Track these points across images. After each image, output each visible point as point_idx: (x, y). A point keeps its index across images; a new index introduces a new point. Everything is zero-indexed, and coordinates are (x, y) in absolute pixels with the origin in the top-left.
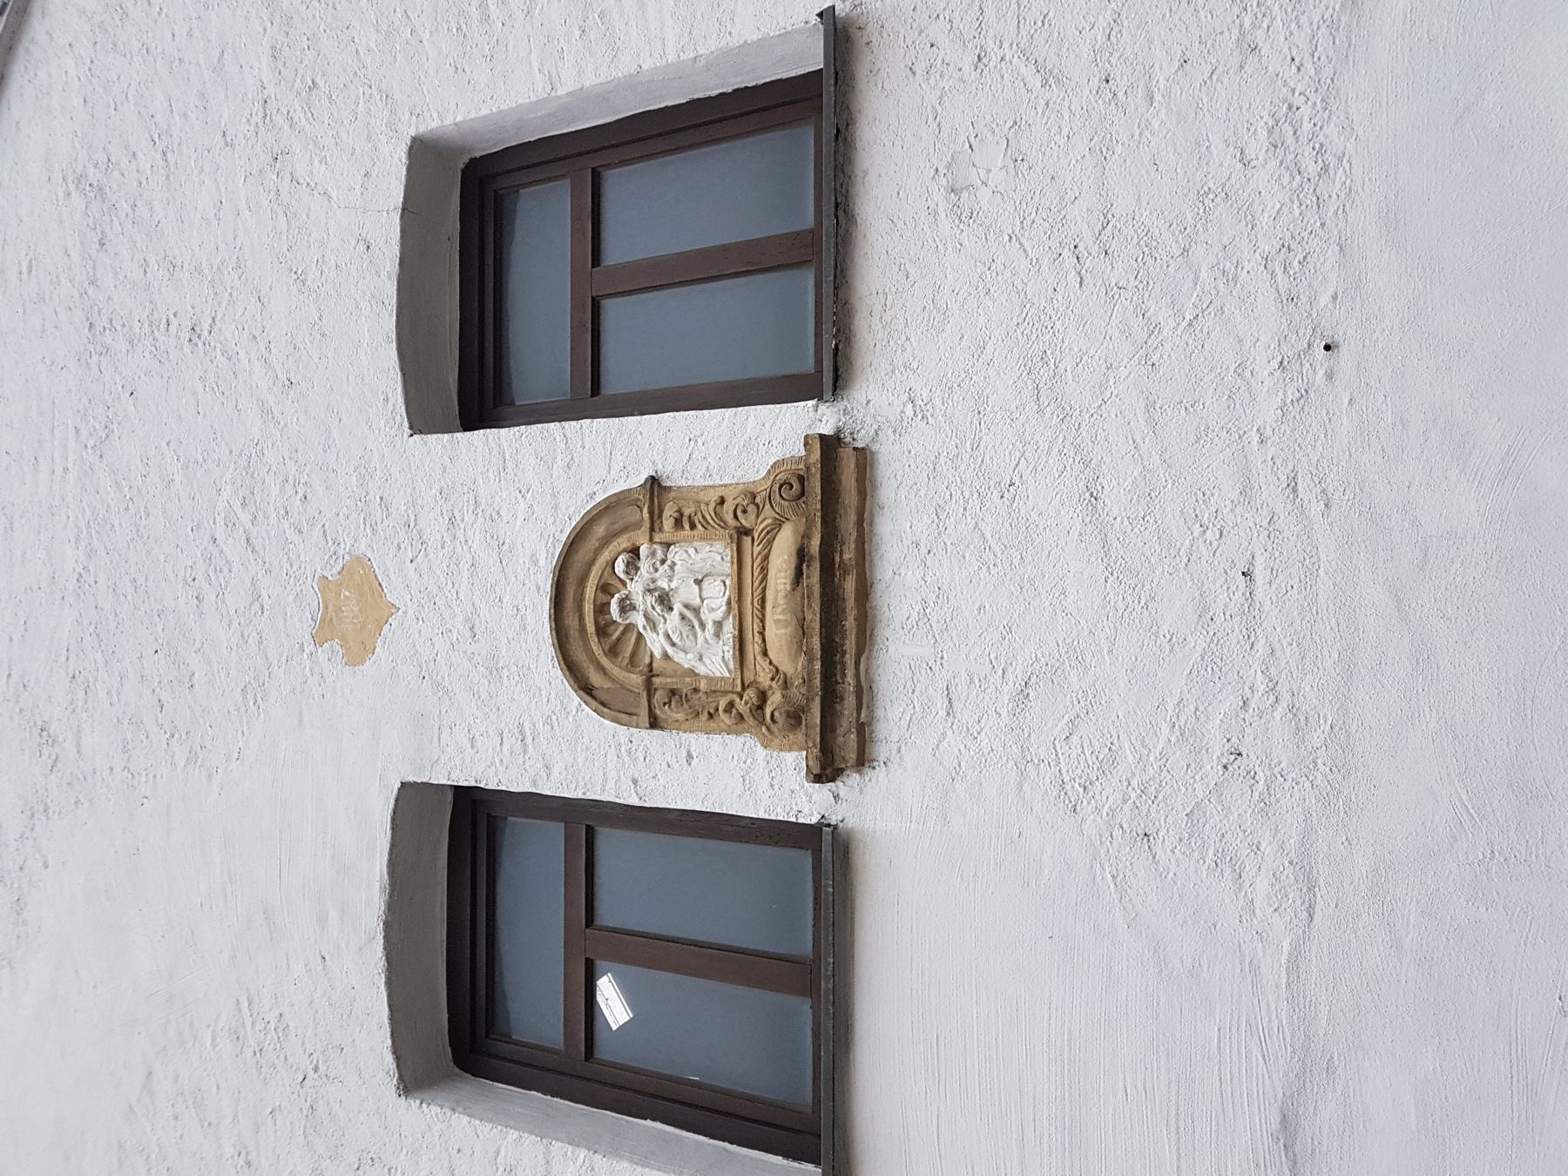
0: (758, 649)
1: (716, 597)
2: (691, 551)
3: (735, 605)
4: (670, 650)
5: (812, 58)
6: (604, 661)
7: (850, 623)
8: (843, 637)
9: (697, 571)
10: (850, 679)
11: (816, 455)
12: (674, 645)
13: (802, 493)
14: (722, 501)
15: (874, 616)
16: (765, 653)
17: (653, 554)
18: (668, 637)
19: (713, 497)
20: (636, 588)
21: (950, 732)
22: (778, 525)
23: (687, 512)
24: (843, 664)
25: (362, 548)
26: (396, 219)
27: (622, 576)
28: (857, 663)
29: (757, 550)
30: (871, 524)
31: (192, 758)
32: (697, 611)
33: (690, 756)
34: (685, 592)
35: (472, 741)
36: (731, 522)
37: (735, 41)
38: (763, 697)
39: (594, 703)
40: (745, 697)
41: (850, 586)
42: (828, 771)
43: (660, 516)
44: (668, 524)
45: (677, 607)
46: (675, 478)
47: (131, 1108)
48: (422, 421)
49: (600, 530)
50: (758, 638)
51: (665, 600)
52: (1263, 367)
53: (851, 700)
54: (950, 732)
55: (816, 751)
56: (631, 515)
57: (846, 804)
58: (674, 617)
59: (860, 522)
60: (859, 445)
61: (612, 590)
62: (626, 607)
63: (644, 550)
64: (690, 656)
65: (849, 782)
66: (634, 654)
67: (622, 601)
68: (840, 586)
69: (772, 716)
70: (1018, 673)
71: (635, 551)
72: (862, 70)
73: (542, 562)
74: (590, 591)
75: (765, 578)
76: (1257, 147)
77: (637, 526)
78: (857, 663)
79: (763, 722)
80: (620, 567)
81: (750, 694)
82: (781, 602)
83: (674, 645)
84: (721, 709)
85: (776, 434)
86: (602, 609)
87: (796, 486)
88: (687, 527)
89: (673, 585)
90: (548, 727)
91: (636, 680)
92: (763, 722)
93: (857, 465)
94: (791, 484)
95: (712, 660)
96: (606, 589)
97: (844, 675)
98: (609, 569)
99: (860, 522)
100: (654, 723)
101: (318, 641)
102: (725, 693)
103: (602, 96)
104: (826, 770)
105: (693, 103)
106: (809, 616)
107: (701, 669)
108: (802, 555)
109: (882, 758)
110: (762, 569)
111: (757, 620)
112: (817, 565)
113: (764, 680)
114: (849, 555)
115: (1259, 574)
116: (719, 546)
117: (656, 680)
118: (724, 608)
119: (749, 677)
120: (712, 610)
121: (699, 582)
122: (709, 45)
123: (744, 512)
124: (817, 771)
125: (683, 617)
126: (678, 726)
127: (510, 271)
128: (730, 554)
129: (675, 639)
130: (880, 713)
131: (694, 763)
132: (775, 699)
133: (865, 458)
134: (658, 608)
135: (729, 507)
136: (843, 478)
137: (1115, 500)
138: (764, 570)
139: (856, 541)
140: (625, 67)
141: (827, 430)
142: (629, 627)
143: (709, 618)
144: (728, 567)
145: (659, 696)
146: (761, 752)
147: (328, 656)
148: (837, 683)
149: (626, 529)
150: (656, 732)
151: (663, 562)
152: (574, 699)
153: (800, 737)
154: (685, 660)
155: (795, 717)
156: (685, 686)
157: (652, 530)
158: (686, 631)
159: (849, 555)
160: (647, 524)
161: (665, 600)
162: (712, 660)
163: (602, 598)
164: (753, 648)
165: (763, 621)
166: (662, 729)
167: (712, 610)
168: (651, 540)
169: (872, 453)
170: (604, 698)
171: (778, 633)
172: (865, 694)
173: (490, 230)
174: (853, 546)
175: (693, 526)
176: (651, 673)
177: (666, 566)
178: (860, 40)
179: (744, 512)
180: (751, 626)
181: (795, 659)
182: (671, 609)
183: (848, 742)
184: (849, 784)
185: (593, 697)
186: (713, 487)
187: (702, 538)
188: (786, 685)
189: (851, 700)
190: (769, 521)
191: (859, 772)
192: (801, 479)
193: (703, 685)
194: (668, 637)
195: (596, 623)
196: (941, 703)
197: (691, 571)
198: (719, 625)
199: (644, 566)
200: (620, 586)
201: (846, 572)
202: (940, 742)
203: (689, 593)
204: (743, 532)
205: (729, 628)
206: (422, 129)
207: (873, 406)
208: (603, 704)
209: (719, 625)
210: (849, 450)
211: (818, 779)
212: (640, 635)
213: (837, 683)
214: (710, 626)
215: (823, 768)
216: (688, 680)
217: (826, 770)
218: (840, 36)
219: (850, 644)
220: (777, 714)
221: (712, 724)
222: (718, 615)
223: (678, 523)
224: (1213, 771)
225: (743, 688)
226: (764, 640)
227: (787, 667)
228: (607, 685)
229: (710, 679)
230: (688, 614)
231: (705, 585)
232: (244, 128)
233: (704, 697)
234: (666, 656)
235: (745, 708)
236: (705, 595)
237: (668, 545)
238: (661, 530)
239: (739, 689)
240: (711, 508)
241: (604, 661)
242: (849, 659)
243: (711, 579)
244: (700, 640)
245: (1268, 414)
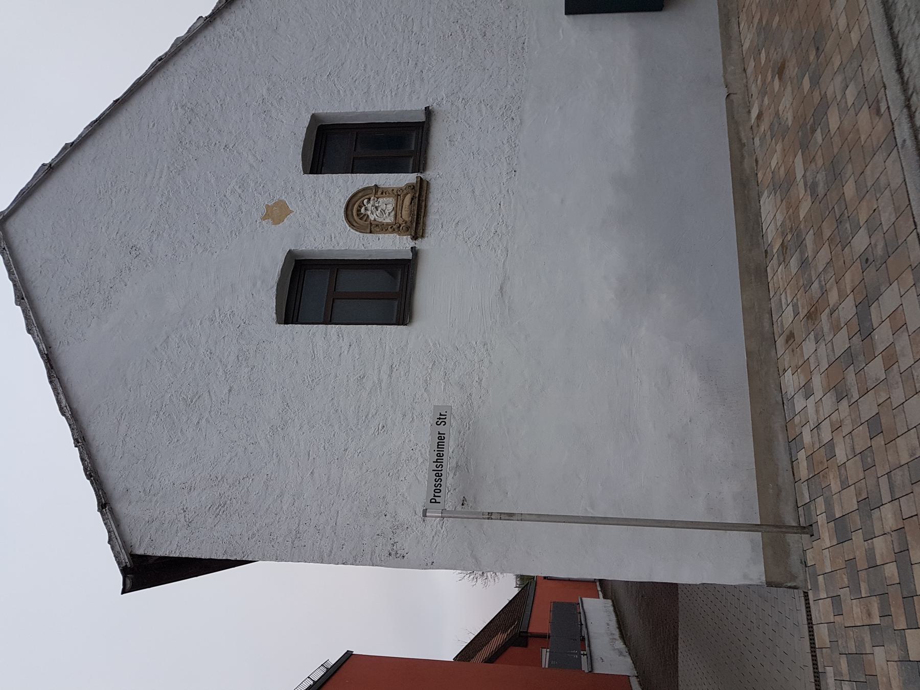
13: (521, 124)
31: (205, 250)
48: (305, 173)
52: (504, 173)
56: (369, 192)
57: (420, 244)
62: (366, 209)
70: (456, 221)
71: (369, 199)
72: (433, 119)
74: (356, 206)
85: (410, 178)
94: (411, 187)
100: (371, 232)
101: (264, 218)
103: (364, 114)
113: (401, 222)
126: (377, 232)
127: (332, 145)
137: (477, 193)
143: (387, 212)
155: (408, 229)
171: (405, 214)
180: (399, 212)
218: (428, 112)
224: (492, 235)
232: (254, 103)
235: (395, 228)
245: (505, 180)
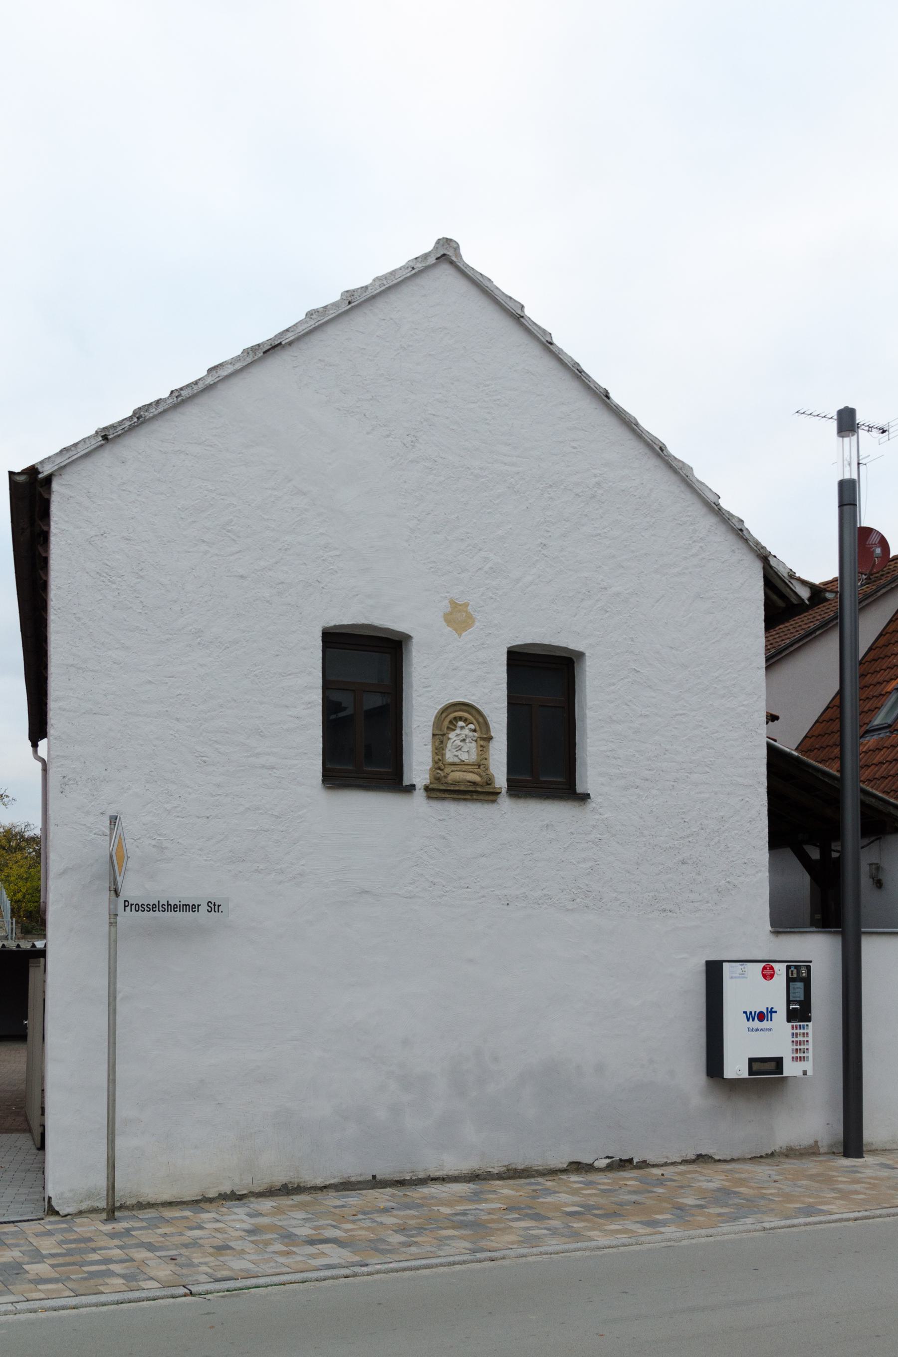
1: (464, 757)
5: (579, 789)
20: (466, 731)
22: (481, 776)
25: (477, 624)
26: (564, 645)
37: (589, 768)
38: (442, 770)
41: (468, 797)
44: (482, 743)
47: (290, 480)
49: (481, 720)
58: (458, 743)
62: (462, 728)
63: (476, 734)
71: (475, 731)
76: (545, 892)
86: (461, 719)
94: (489, 782)
96: (465, 720)
100: (434, 735)
104: (427, 789)
105: (575, 759)
115: (469, 890)
122: (589, 761)
126: (434, 742)
133: (494, 801)
140: (589, 733)
146: (429, 767)
147: (445, 606)
154: (449, 745)
155: (438, 779)
161: (464, 740)
164: (453, 768)
172: (444, 799)
173: (801, 643)
178: (582, 803)
180: (458, 768)
183: (434, 795)
184: (424, 794)
188: (445, 777)
189: (444, 796)
196: (441, 818)
199: (471, 734)
203: (465, 749)
204: (479, 766)
206: (587, 658)
207: (505, 803)
214: (456, 753)
217: (427, 789)
223: (482, 746)
234: (449, 739)
235: (439, 764)
245: (497, 892)
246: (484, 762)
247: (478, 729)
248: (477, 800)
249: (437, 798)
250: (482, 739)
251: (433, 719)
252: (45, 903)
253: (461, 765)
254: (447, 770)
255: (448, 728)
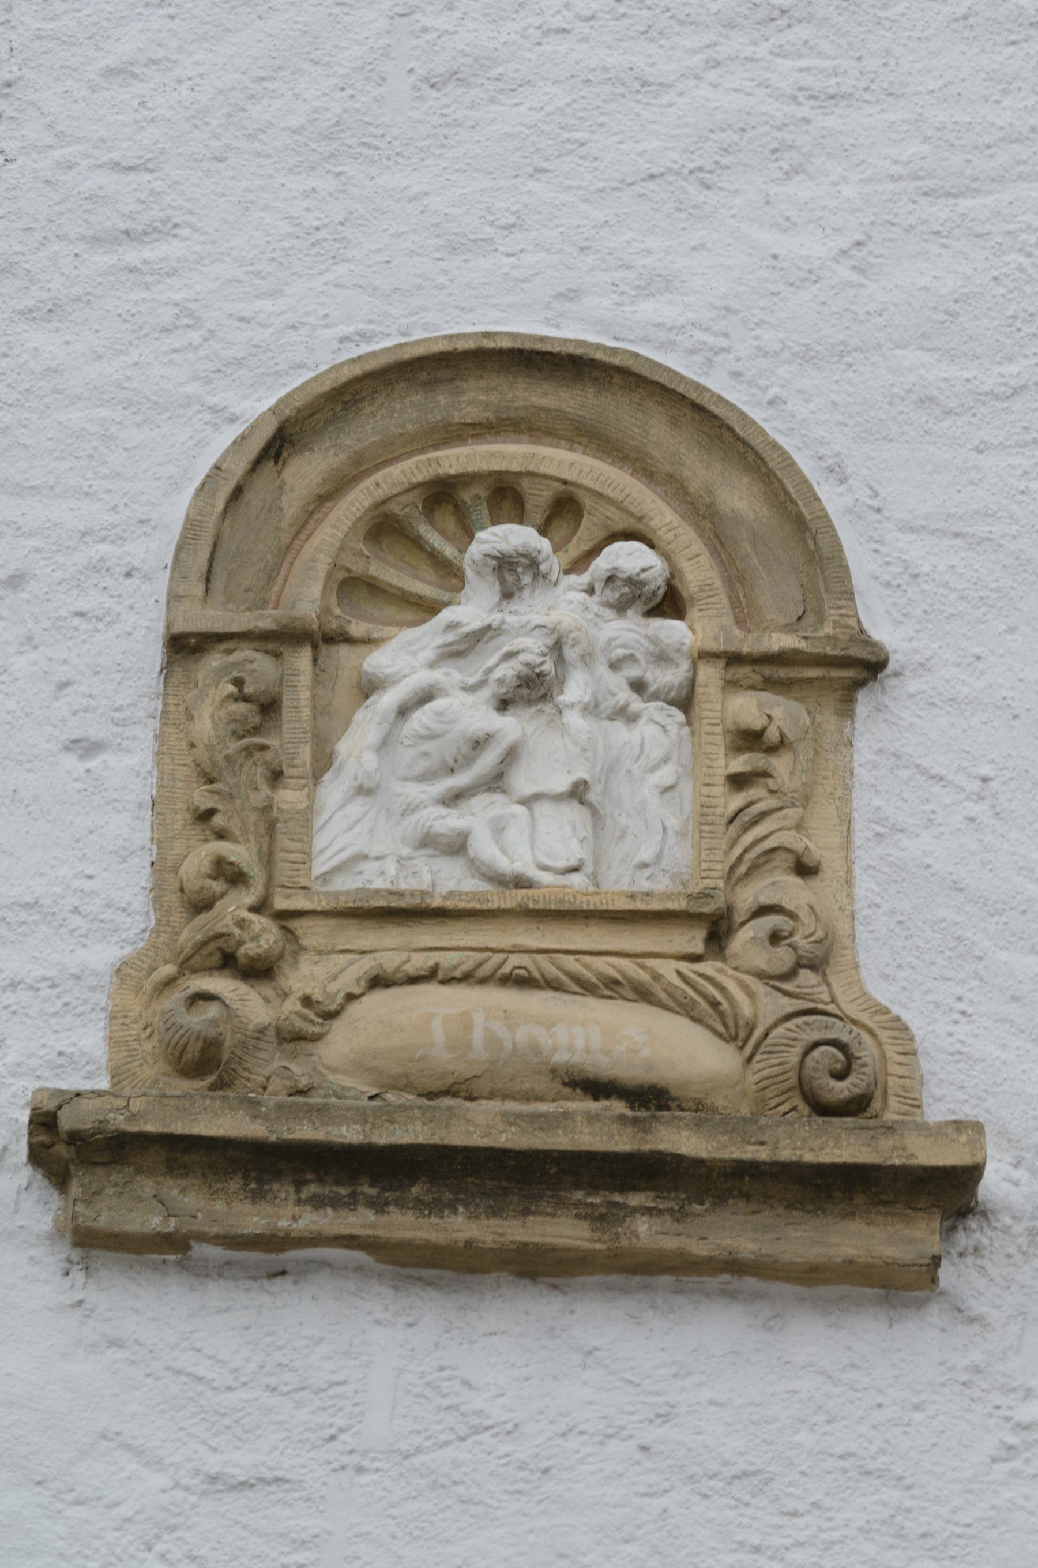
0: (389, 962)
1: (533, 844)
2: (666, 775)
3: (513, 898)
4: (388, 700)
6: (358, 500)
7: (460, 1227)
8: (420, 1206)
9: (611, 795)
10: (312, 1221)
11: (929, 1154)
12: (403, 711)
14: (805, 869)
15: (624, 1290)
16: (378, 982)
17: (662, 658)
18: (425, 697)
19: (819, 845)
20: (564, 604)
21: (162, 1480)
22: (734, 1032)
23: (780, 765)
24: (351, 1203)
27: (602, 563)
28: (350, 1241)
29: (668, 969)
30: (729, 1294)
32: (496, 782)
33: (86, 748)
34: (553, 750)
35: (122, 72)
36: (746, 897)
38: (259, 971)
39: (239, 467)
40: (259, 922)
41: (561, 1230)
42: (62, 1150)
43: (770, 684)
44: (748, 708)
45: (510, 726)
46: (880, 734)
49: (738, 498)
50: (419, 962)
51: (531, 690)
53: (253, 1218)
54: (162, 1480)
55: (120, 1122)
56: (776, 593)
58: (475, 715)
59: (734, 1266)
60: (946, 1274)
61: (561, 528)
62: (511, 572)
63: (673, 631)
64: (370, 760)
65: (29, 1203)
66: (374, 588)
67: (533, 563)
68: (561, 1204)
69: (208, 997)
71: (669, 603)
73: (648, 309)
75: (587, 988)
77: (743, 613)
78: (350, 1241)
79: (188, 965)
80: (629, 557)
81: (263, 937)
82: (522, 1036)
83: (403, 711)
84: (223, 848)
86: (506, 496)
87: (841, 1090)
88: (740, 764)
89: (574, 719)
90: (167, 315)
91: (307, 598)
92: (188, 965)
93: (890, 1264)
95: (358, 831)
96: (564, 508)
97: (318, 1203)
98: (622, 523)
99: (734, 1266)
100: (183, 647)
102: (268, 859)
106: (484, 1111)
107: (333, 790)
108: (650, 1098)
109: (92, 1295)
110: (613, 984)
111: (468, 961)
112: (623, 1142)
113: (307, 977)
114: (646, 1232)
116: (681, 855)
117: (302, 659)
118: (505, 865)
119: (314, 934)
120: (498, 829)
121: (578, 793)
123: (775, 938)
124: (66, 1122)
125: (479, 744)
126: (174, 717)
128: (661, 888)
129: (421, 718)
130: (215, 1292)
131: (71, 762)
132: (252, 1005)
133: (905, 1286)
134: (508, 671)
135: (791, 891)
136: (855, 1225)
138: (610, 988)
139: (682, 1253)
141: (993, 1185)
142: (451, 574)
143: (476, 818)
144: (620, 882)
145: (259, 667)
146: (104, 956)
148: (299, 1184)
149: (735, 577)
150: (155, 652)
151: (638, 686)
152: (257, 403)
153: (151, 1070)
155: (205, 1062)
156: (290, 740)
157: (733, 659)
158: (444, 749)
159: (646, 1232)
160: (748, 646)
161: (531, 690)
162: (358, 831)
163: (538, 498)
164: (393, 947)
165: (466, 978)
166: (168, 667)
167: (498, 829)
168: (705, 655)
169: (920, 1304)
170: (253, 499)
172: (269, 1257)
174: (669, 1243)
175: (738, 781)
176: (324, 639)
177: (625, 695)
179: (775, 938)
181: (360, 1066)
182: (504, 705)
183: (141, 1205)
185: (257, 464)
186: (847, 844)
187: (704, 813)
188: (292, 1039)
189: (253, 1218)
190: (746, 1009)
191: (58, 1233)
192: (857, 1106)
193: (289, 797)
194: (425, 697)
195: (466, 479)
196: (240, 1461)
197: (611, 769)
198: (457, 846)
199: (630, 630)
200: (575, 549)
201: (599, 1219)
202: (138, 1452)
203: (547, 768)
204: (718, 931)
205: (446, 880)
208: (238, 492)
209: (457, 846)
210: (934, 1244)
211: (44, 1122)
212: (430, 608)
213: (299, 1184)
214: (449, 821)
215: (75, 1138)
216: (305, 754)
219: (402, 1224)
220: (212, 1010)
221: (180, 819)
222: (485, 847)
223: (749, 739)
225: (284, 916)
226: (414, 980)
227: (340, 1043)
228: (291, 505)
229: (306, 819)
230: (487, 761)
231: (573, 812)
233: (258, 799)
234: (368, 688)
236: (543, 809)
237: (685, 702)
238: (731, 685)
239: (280, 903)
240: (788, 838)
241: (358, 500)
242: (360, 1221)
243: (585, 830)
244: (415, 791)
246: (780, 886)
247: (699, 573)
248: (639, 1270)
249: (168, 1249)
250: (771, 671)
251: (178, 507)
252: (398, 588)
253: (520, 932)
254: (318, 971)
255: (352, 586)
